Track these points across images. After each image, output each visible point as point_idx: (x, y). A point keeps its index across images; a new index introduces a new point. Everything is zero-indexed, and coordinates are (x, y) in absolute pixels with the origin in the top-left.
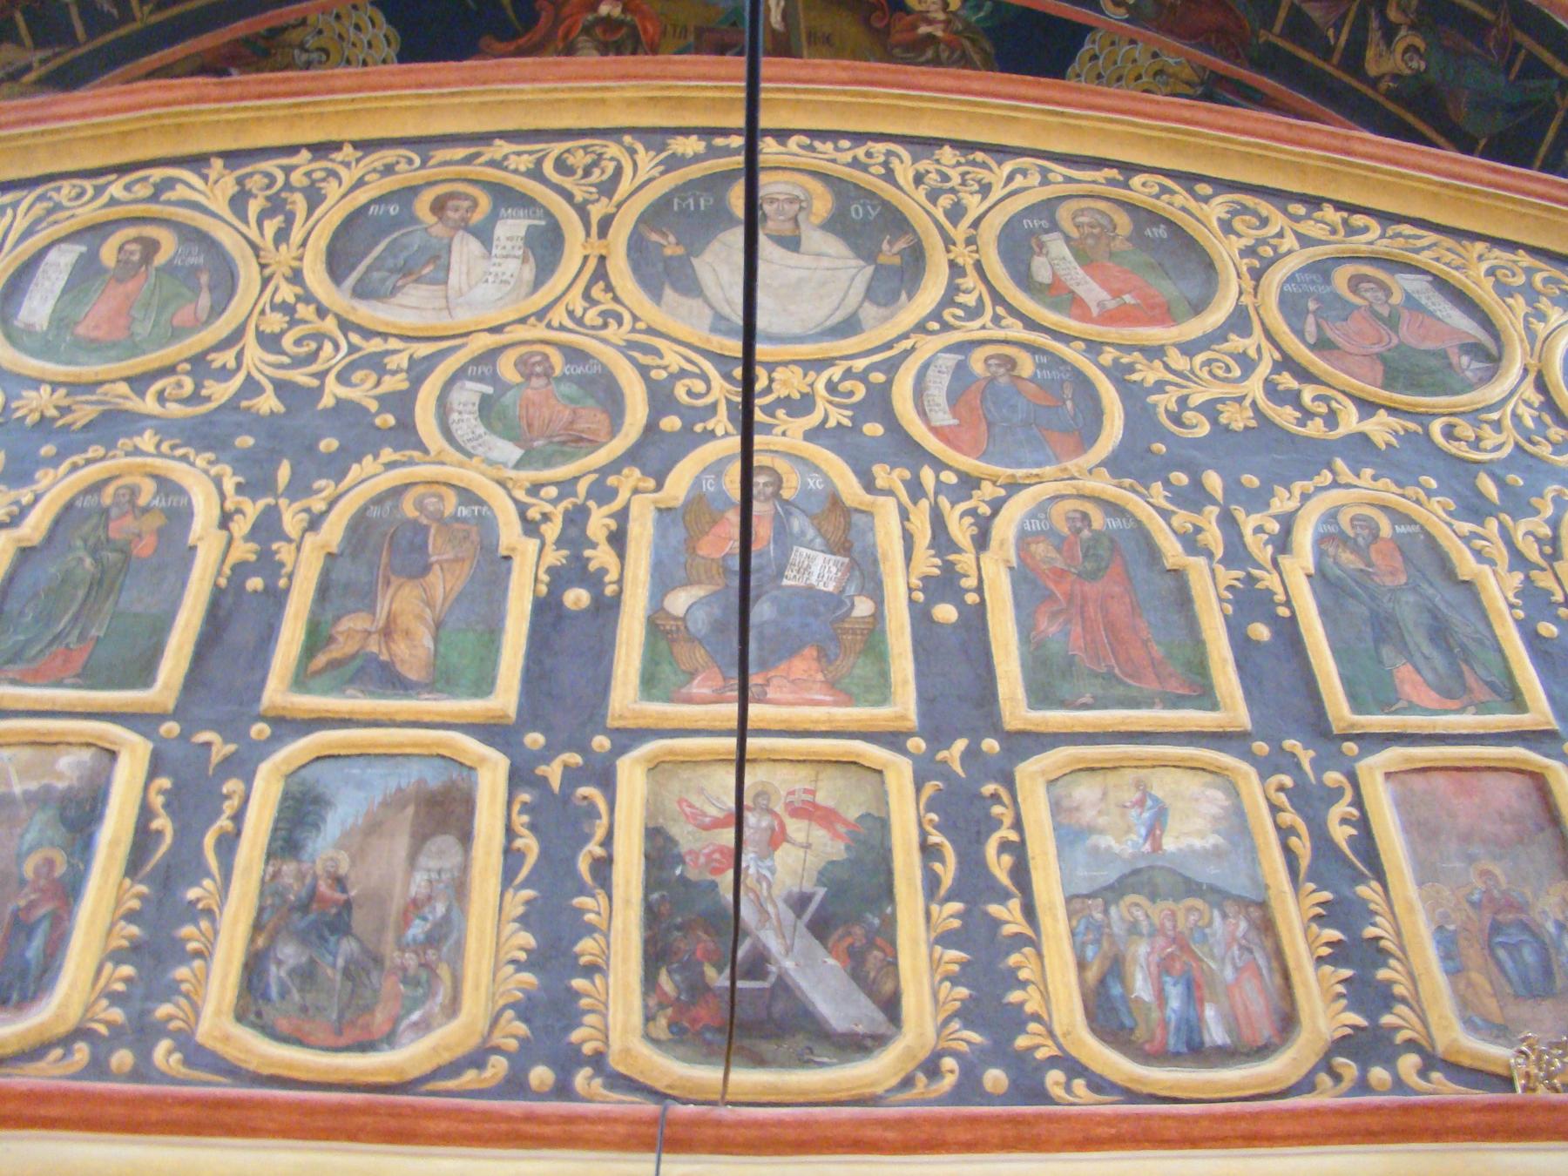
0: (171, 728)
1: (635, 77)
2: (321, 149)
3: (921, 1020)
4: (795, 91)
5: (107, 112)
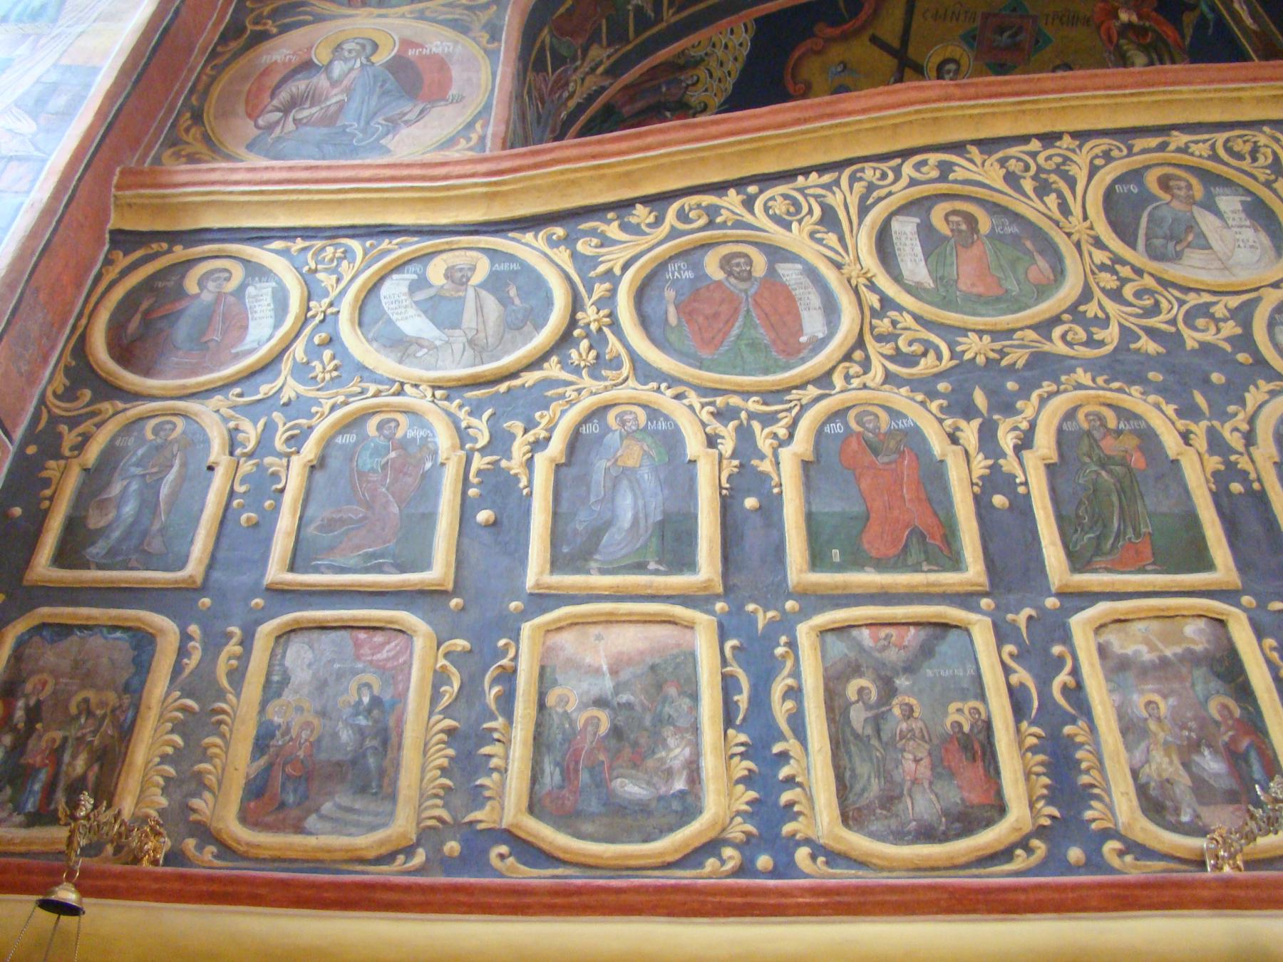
0: (1051, 602)
2: (1049, 138)
3: (1018, 816)
5: (881, 108)
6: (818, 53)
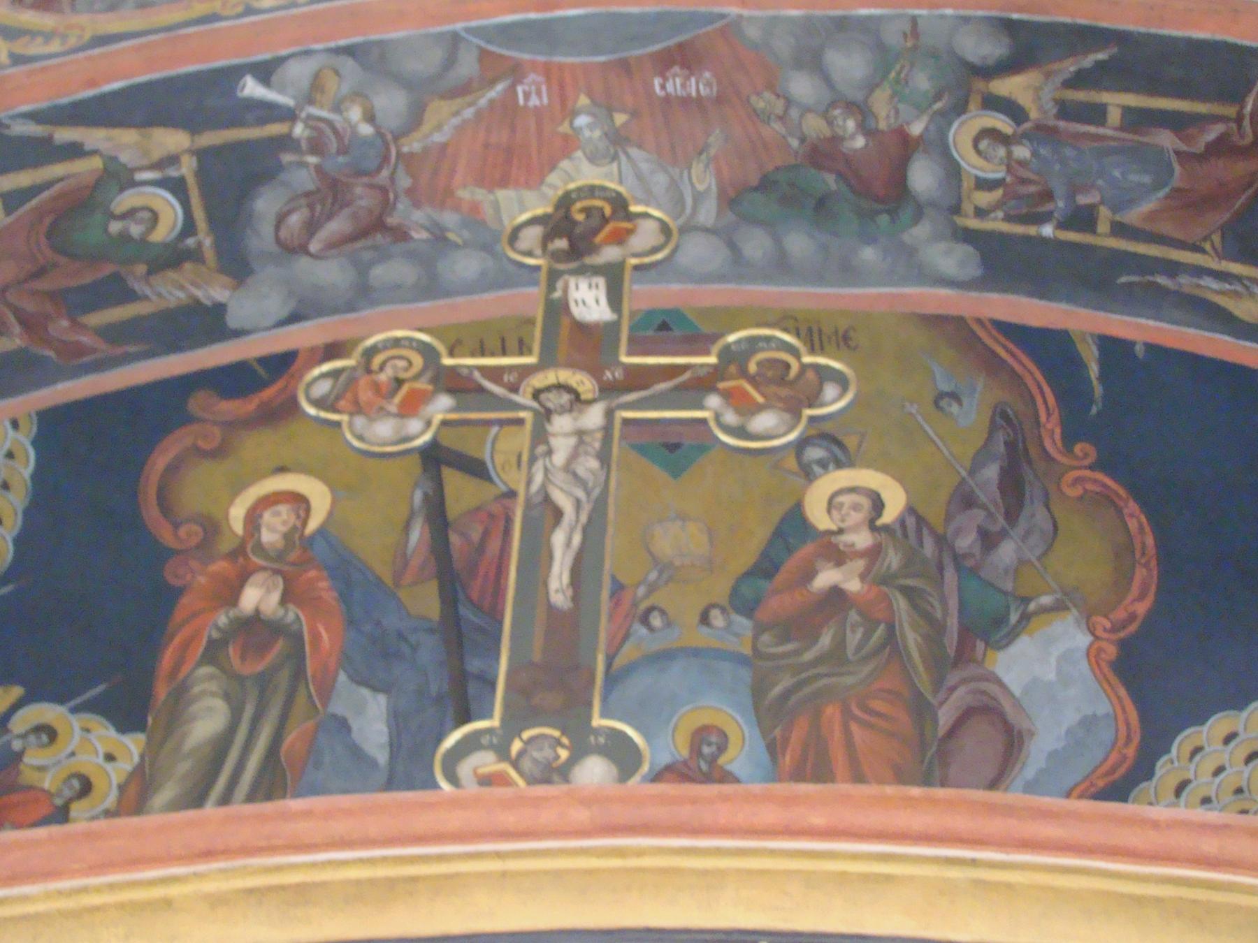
1: (227, 853)
4: (499, 855)
6: (219, 453)
